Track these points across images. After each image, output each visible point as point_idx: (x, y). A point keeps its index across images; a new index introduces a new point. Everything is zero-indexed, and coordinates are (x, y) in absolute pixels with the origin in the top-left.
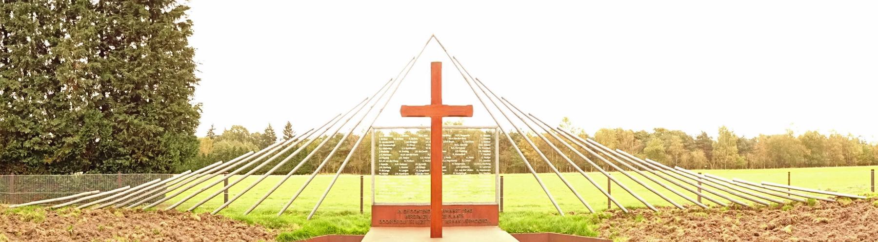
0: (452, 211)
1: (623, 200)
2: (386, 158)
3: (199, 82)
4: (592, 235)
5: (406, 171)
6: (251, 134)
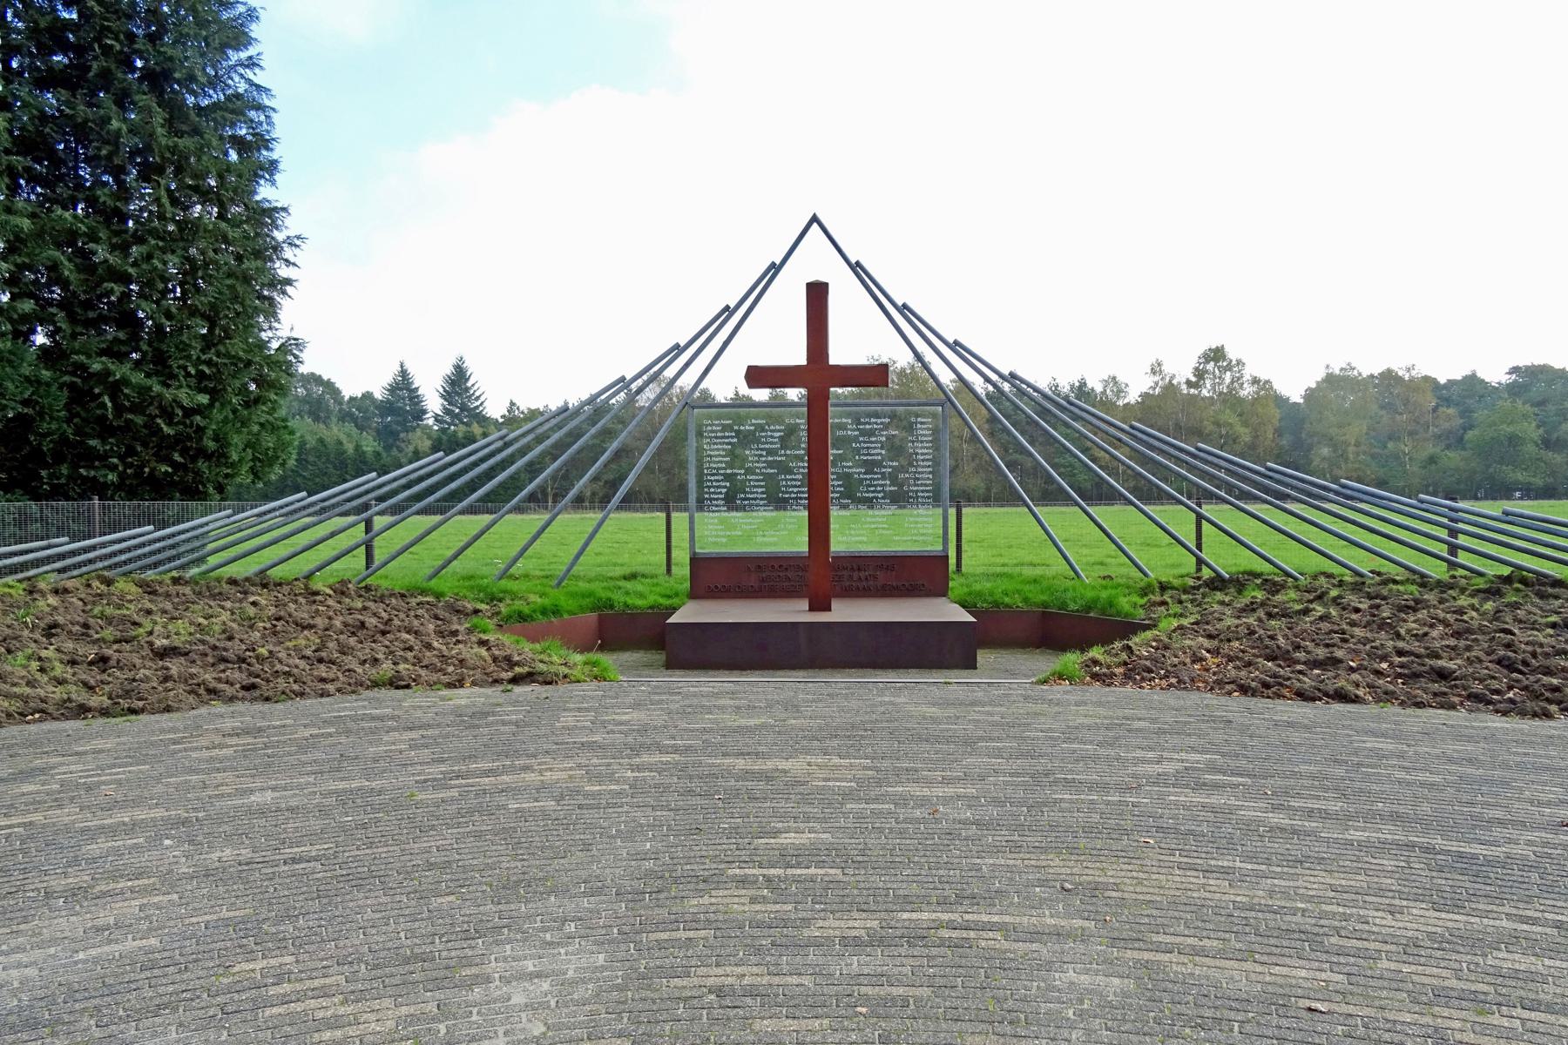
0: (855, 567)
1: (1224, 558)
2: (720, 465)
3: (289, 289)
4: (1127, 615)
6: (346, 398)
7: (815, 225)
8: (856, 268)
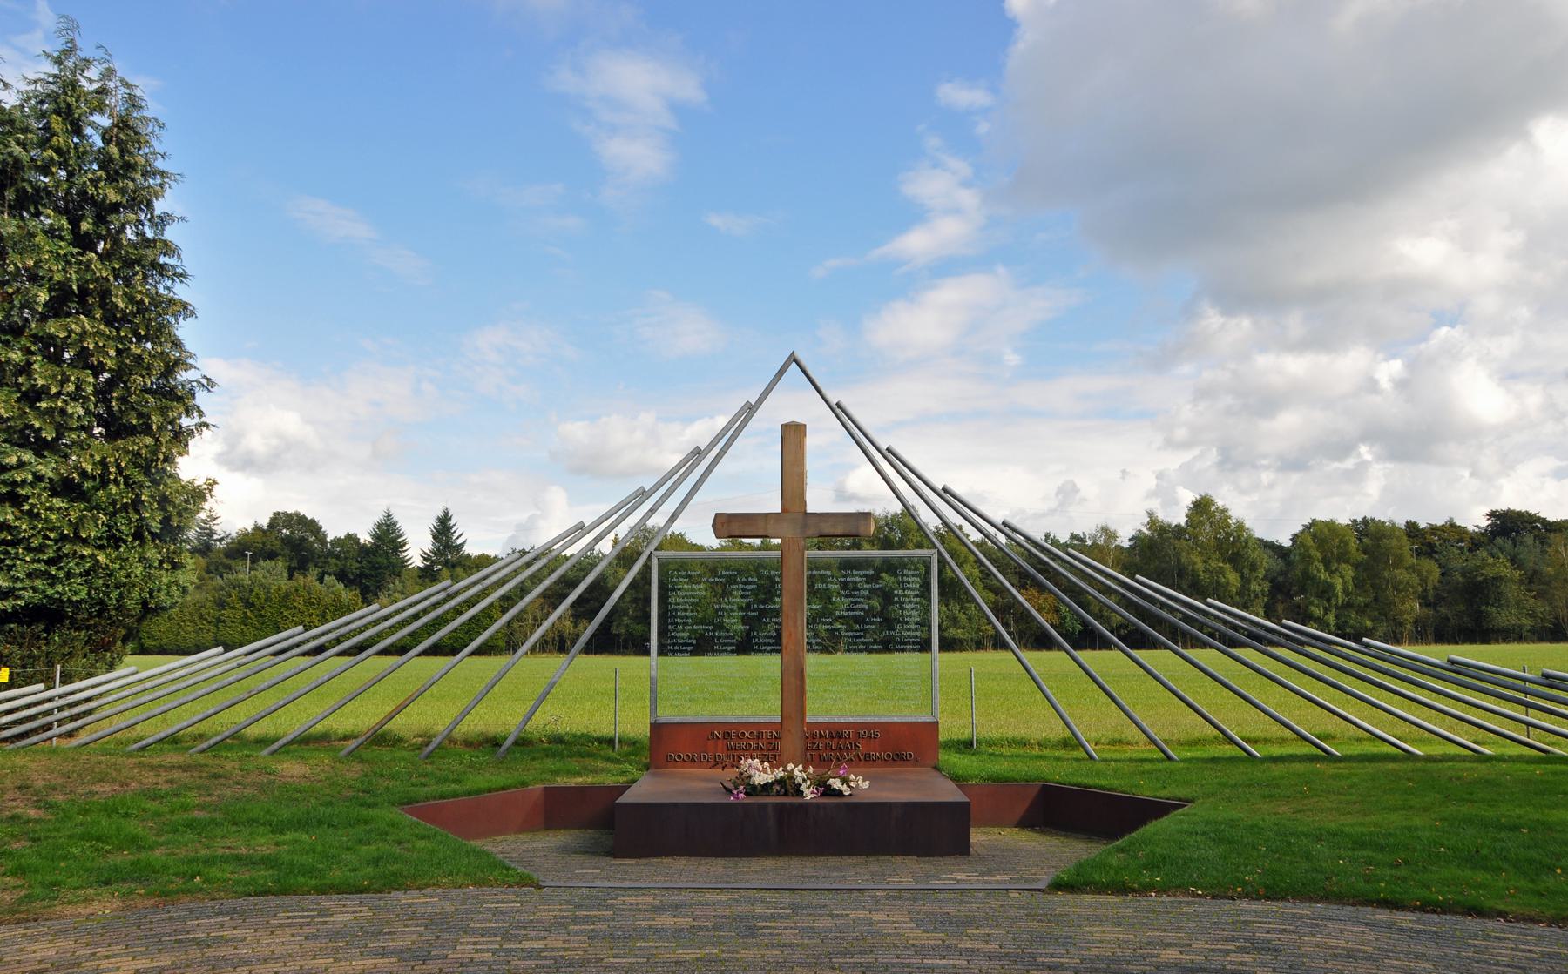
5: (729, 648)
8: (838, 410)
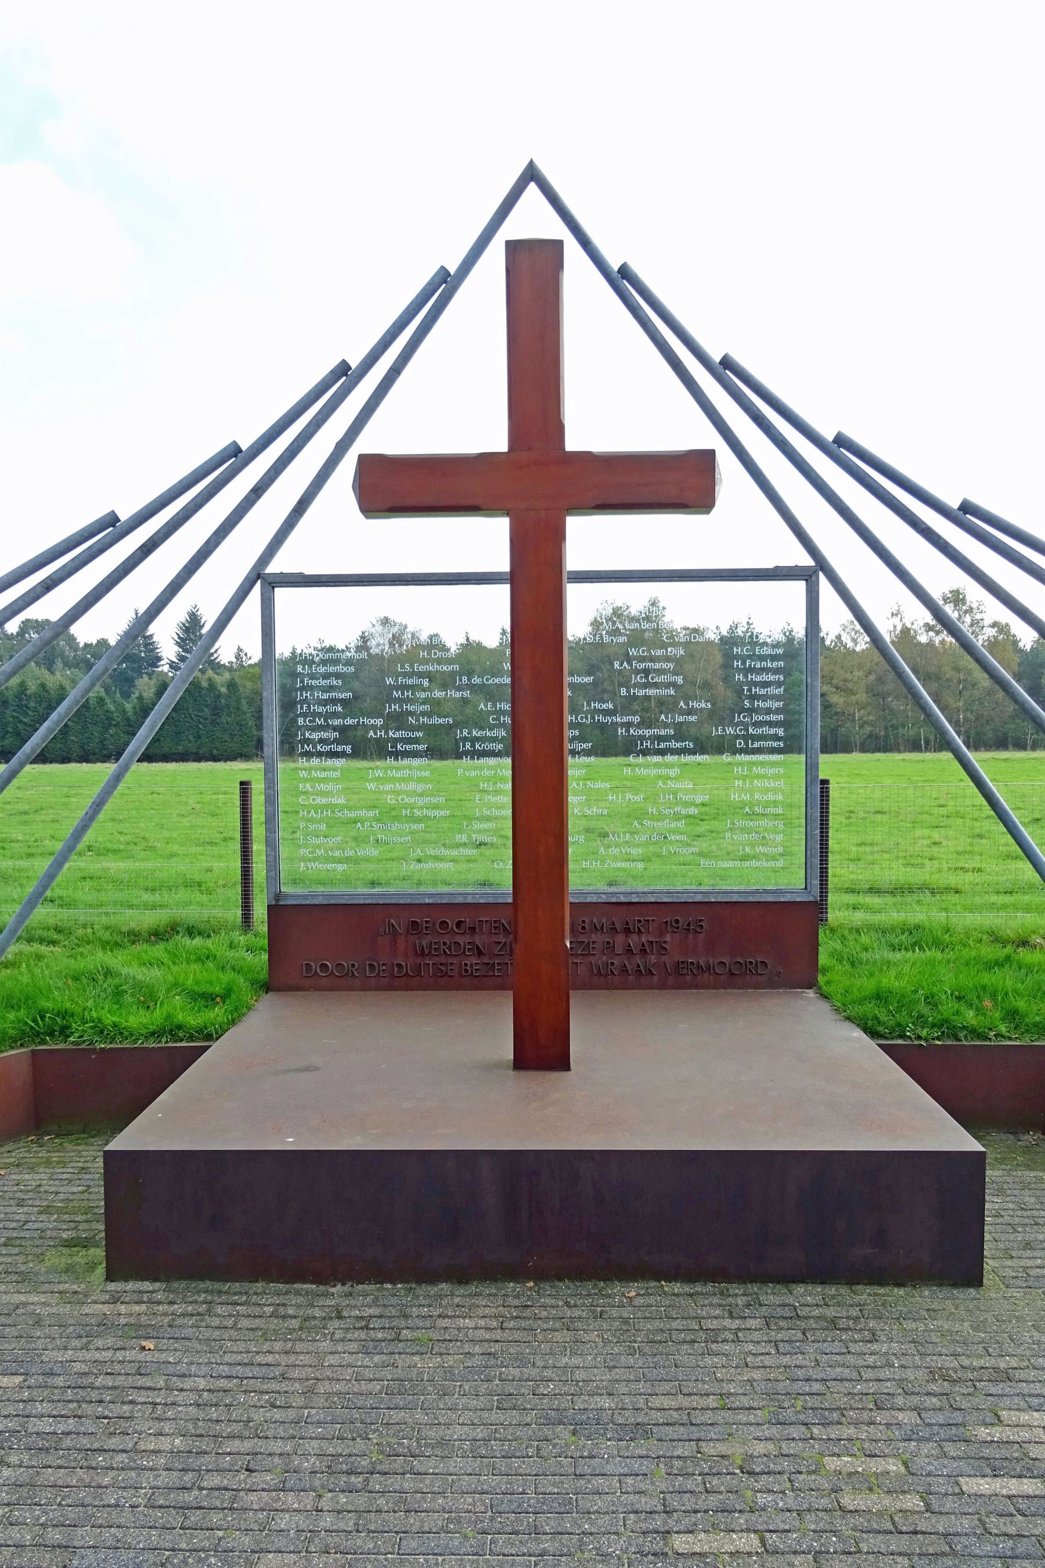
0: (618, 926)
6: (81, 645)
7: (532, 188)
